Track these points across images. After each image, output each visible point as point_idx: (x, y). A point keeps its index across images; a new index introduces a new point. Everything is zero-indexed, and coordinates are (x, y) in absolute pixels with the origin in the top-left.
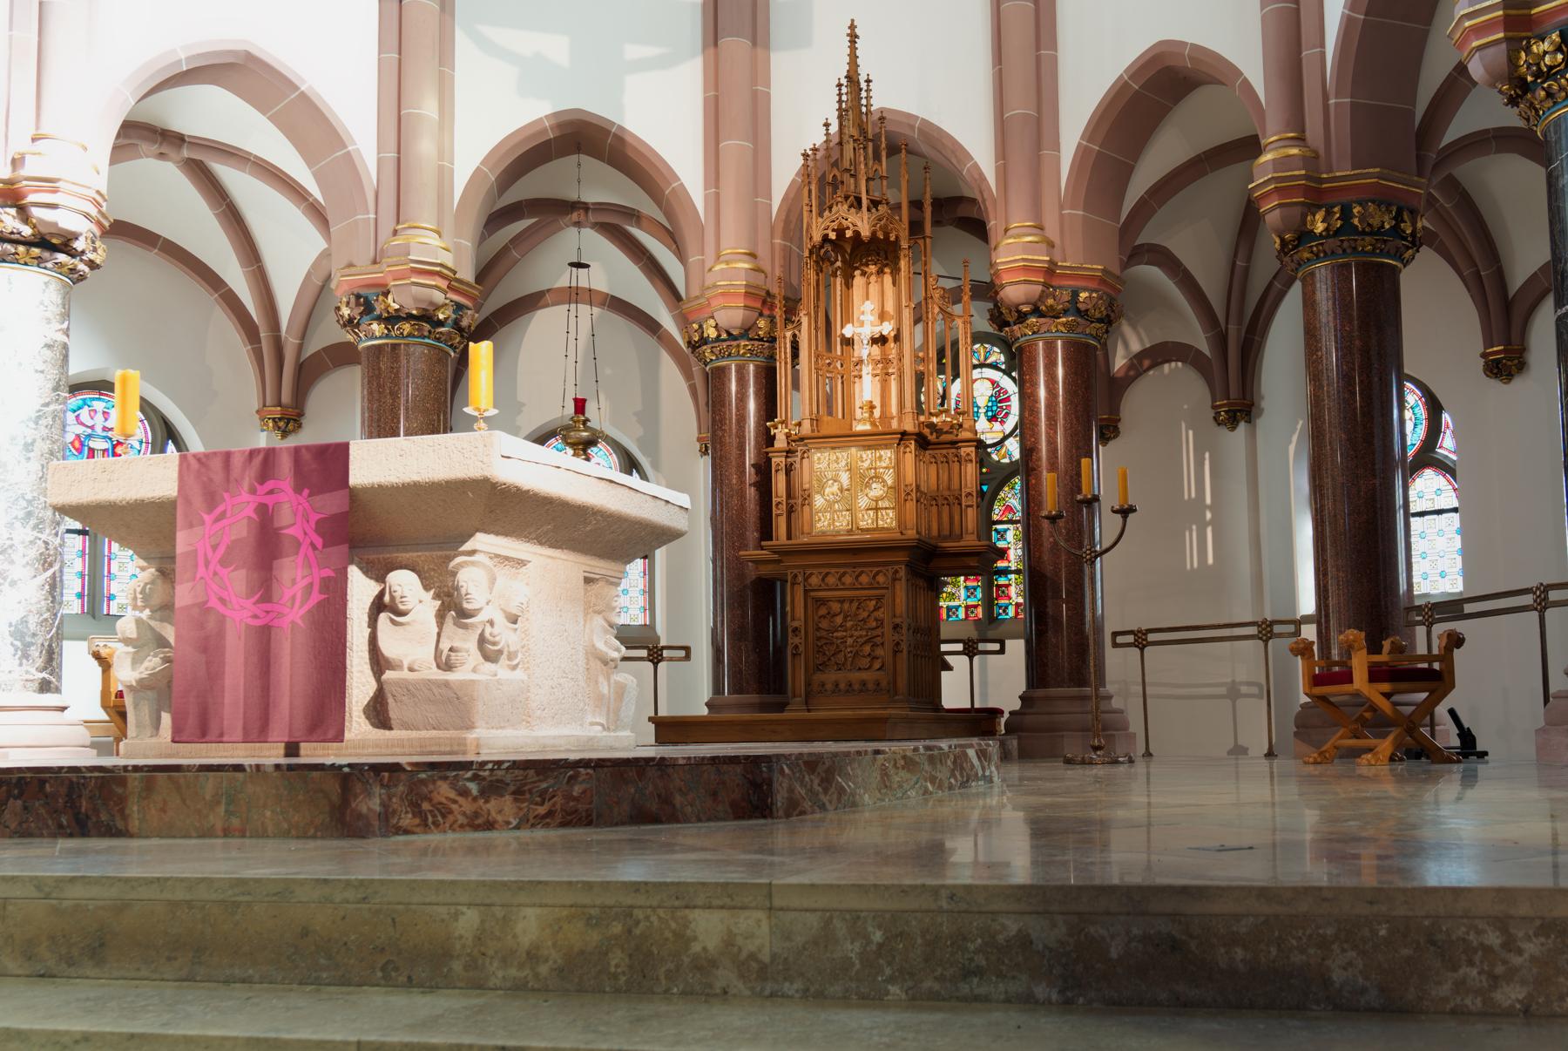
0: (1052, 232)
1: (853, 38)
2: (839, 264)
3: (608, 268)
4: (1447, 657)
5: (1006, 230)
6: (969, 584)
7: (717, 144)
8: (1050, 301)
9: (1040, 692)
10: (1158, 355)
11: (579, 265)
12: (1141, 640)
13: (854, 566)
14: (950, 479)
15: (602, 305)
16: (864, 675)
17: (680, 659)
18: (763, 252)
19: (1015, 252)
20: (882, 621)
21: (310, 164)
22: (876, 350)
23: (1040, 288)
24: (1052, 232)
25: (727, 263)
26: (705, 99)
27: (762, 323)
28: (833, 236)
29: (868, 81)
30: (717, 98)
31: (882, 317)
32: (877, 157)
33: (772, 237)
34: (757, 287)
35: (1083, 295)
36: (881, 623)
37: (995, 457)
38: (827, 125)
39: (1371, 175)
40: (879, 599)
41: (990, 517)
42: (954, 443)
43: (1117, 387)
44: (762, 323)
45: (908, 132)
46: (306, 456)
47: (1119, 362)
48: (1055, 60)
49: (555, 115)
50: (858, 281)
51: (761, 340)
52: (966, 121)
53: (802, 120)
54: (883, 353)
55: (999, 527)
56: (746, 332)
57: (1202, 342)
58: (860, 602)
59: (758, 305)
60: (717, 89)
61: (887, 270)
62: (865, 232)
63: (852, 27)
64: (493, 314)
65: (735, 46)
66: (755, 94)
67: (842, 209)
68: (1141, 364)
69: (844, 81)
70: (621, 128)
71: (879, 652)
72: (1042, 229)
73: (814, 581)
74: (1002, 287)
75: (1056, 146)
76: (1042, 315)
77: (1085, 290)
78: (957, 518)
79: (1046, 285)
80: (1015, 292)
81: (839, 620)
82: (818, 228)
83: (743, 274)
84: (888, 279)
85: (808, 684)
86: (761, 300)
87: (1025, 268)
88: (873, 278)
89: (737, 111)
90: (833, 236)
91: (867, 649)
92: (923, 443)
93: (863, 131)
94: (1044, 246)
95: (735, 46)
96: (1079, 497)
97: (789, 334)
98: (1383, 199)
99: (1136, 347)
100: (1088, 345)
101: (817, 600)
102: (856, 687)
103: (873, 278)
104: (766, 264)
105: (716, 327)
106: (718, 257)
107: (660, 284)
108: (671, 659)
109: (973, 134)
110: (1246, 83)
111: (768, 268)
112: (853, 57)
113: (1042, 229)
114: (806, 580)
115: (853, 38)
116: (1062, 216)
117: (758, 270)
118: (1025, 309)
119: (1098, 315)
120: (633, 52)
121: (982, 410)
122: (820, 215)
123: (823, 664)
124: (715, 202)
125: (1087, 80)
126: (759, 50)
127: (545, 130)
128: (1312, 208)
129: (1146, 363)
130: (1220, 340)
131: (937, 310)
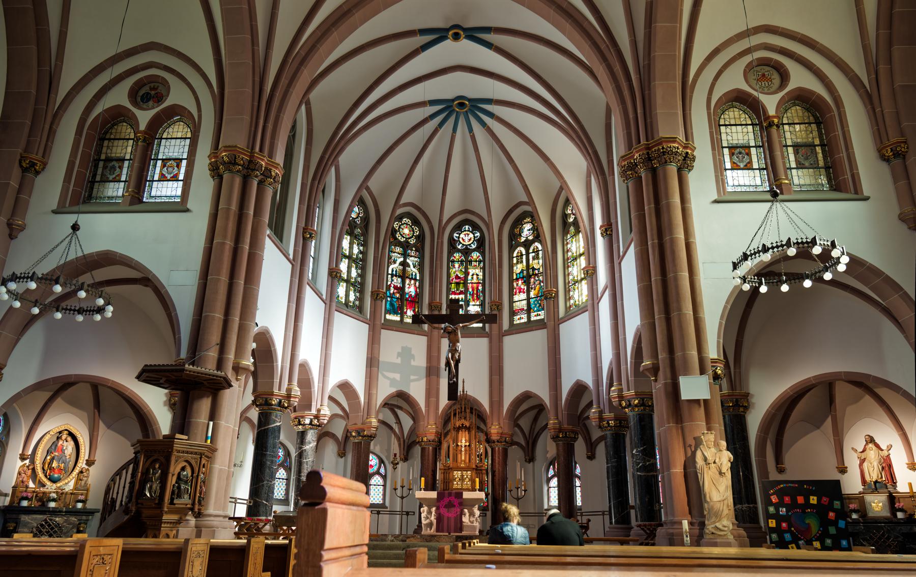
4: (588, 523)
39: (570, 427)
46: (225, 385)
57: (523, 443)
65: (434, 378)
89: (431, 392)
98: (573, 431)
110: (189, 112)
120: (412, 377)
124: (428, 411)
125: (509, 397)
128: (560, 432)
130: (527, 443)
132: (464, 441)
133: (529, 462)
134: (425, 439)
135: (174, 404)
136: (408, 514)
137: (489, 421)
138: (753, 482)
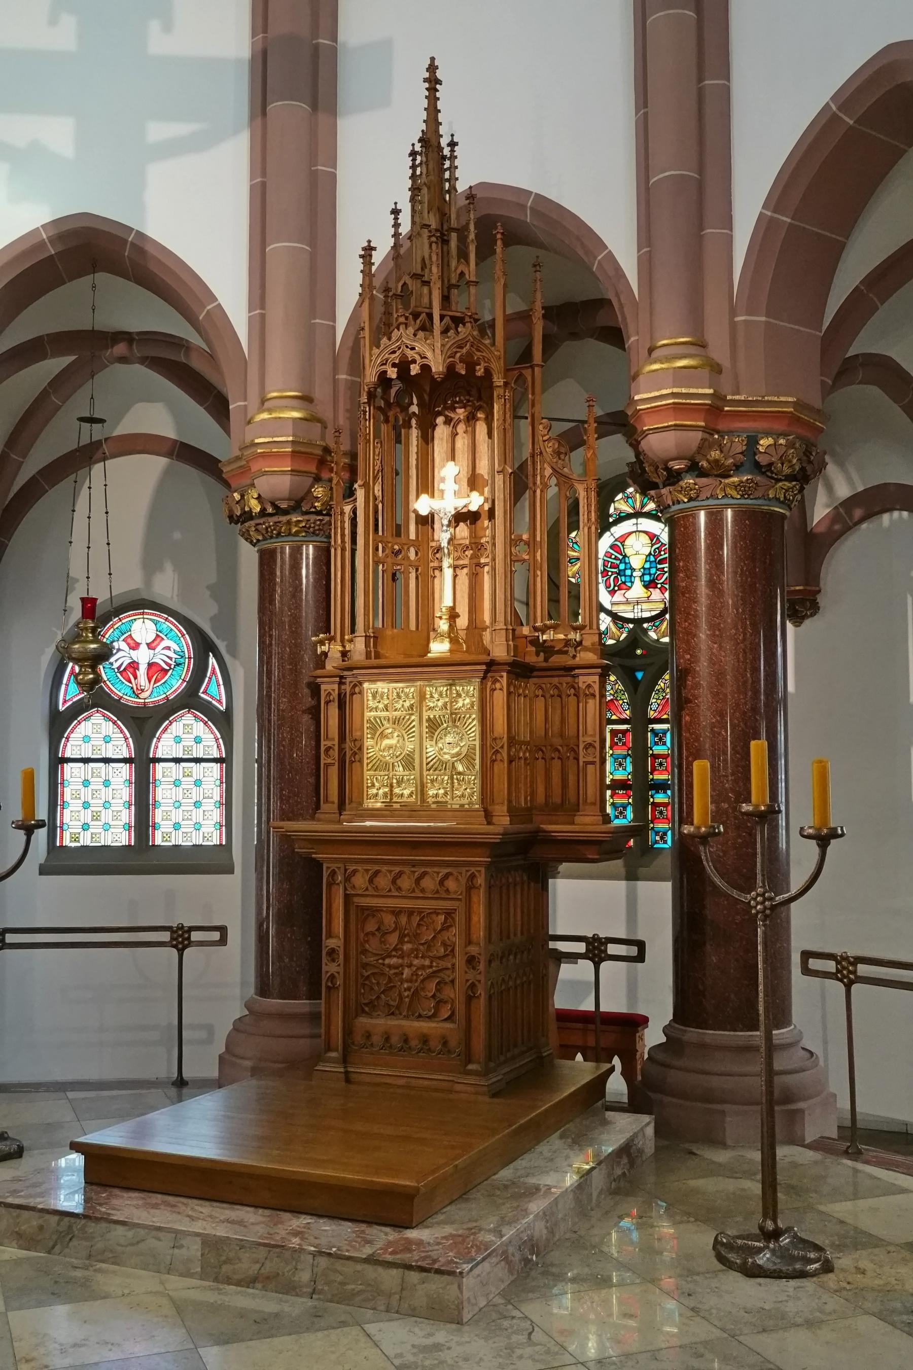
1: (433, 82)
2: (414, 409)
3: (159, 412)
5: (651, 351)
6: (618, 801)
7: (701, 228)
8: (715, 454)
9: (692, 1034)
10: (874, 501)
11: (92, 420)
12: (847, 971)
13: (414, 864)
14: (563, 721)
15: (169, 455)
16: (425, 1026)
18: (322, 393)
19: (661, 381)
22: (463, 531)
23: (699, 435)
24: (719, 352)
26: (252, 188)
27: (319, 491)
29: (453, 144)
31: (474, 482)
32: (463, 255)
33: (335, 370)
34: (310, 444)
35: (765, 442)
37: (653, 635)
38: (396, 212)
40: (449, 914)
41: (646, 713)
42: (568, 670)
43: (816, 546)
44: (319, 491)
45: (515, 214)
47: (820, 512)
48: (726, 93)
49: (55, 222)
50: (441, 431)
51: (319, 513)
52: (598, 191)
53: (372, 207)
54: (475, 536)
55: (657, 727)
56: (297, 504)
58: (425, 916)
59: (313, 468)
60: (264, 174)
62: (438, 367)
63: (432, 68)
64: (40, 472)
67: (404, 335)
68: (850, 514)
69: (418, 148)
70: (140, 235)
72: (704, 346)
73: (360, 881)
74: (645, 434)
75: (728, 222)
76: (702, 473)
77: (767, 434)
78: (572, 778)
79: (708, 430)
81: (393, 939)
82: (377, 362)
83: (290, 428)
84: (481, 428)
85: (348, 1031)
87: (677, 408)
88: (461, 428)
89: (293, 198)
90: (392, 373)
91: (432, 986)
92: (520, 671)
93: (443, 216)
94: (705, 373)
95: (287, 111)
96: (745, 807)
97: (348, 509)
99: (843, 491)
100: (773, 514)
101: (362, 909)
102: (414, 1043)
104: (327, 413)
105: (259, 498)
106: (263, 401)
108: (201, 944)
109: (607, 210)
111: (328, 415)
112: (433, 111)
113: (704, 346)
114: (347, 879)
115: (433, 82)
116: (733, 326)
118: (677, 466)
119: (786, 470)
120: (159, 131)
121: (637, 574)
122: (376, 343)
123: (370, 1003)
124: (259, 326)
126: (322, 117)
127: (41, 245)
129: (858, 513)
131: (548, 471)
136: (181, 939)
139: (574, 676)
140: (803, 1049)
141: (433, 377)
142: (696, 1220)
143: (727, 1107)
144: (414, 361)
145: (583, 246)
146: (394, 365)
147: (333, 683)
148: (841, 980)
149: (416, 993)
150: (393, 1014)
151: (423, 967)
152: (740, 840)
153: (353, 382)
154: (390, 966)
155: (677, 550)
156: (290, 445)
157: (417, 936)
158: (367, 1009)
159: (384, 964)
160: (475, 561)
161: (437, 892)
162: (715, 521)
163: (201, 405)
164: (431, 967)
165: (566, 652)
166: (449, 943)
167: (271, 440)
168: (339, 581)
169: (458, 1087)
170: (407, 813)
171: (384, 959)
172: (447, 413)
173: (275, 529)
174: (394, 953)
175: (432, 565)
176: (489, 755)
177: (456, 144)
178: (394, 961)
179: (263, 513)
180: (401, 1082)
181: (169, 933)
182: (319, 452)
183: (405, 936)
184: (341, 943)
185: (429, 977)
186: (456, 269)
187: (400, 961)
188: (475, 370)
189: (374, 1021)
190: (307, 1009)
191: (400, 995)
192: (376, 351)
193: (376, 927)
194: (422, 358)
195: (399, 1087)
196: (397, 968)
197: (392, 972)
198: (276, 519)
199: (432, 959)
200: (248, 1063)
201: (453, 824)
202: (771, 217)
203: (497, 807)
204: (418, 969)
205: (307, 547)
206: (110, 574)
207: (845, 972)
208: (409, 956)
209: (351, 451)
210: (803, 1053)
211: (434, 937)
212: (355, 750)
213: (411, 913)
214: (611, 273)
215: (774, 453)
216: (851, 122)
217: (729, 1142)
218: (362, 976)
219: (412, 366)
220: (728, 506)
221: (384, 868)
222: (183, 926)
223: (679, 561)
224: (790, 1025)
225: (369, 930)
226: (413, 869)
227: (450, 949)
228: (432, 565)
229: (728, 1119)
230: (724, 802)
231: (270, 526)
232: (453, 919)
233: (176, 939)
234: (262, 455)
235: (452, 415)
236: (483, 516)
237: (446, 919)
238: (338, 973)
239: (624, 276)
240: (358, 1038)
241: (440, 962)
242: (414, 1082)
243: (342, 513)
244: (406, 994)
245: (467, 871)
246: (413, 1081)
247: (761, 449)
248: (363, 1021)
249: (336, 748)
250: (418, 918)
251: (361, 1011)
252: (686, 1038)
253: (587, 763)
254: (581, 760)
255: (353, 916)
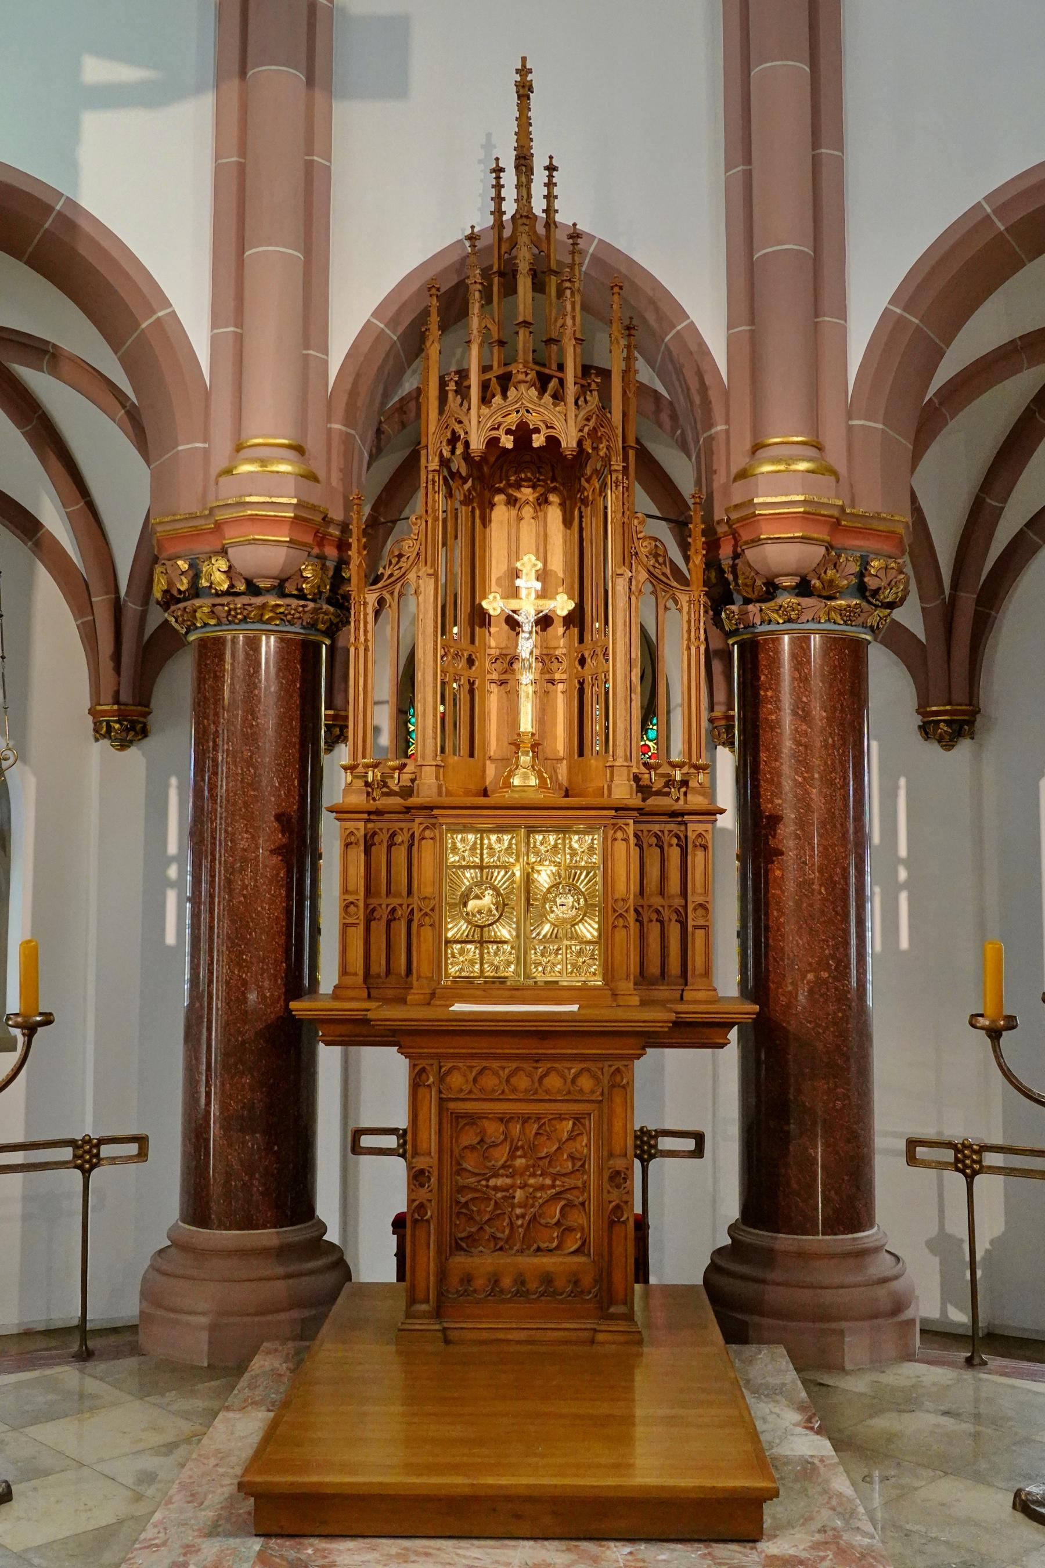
0: (836, 456)
1: (524, 91)
7: (241, 249)
16: (547, 1262)
17: (129, 1159)
20: (584, 1161)
21: (934, 394)
25: (263, 462)
26: (218, 169)
28: (508, 442)
29: (551, 168)
30: (242, 168)
34: (313, 508)
36: (580, 1164)
50: (500, 513)
51: (301, 596)
59: (309, 539)
61: (553, 498)
62: (569, 441)
63: (524, 71)
65: (278, 79)
66: (309, 165)
71: (577, 1218)
73: (456, 1080)
77: (878, 555)
80: (781, 554)
81: (500, 1156)
83: (291, 485)
84: (554, 514)
85: (442, 1275)
86: (312, 526)
89: (787, 249)
90: (508, 442)
91: (555, 1211)
95: (278, 79)
101: (457, 1117)
102: (532, 1285)
103: (528, 511)
106: (239, 448)
107: (53, 459)
108: (113, 1160)
112: (524, 124)
114: (442, 1079)
115: (524, 91)
116: (850, 428)
117: (311, 477)
118: (786, 582)
120: (97, 70)
124: (235, 352)
126: (319, 95)
132: (529, 584)
133: (948, 742)
134: (216, 573)
135: (776, 760)
136: (87, 1155)
137: (730, 430)
138: (882, 936)
139: (685, 824)
140: (887, 1251)
141: (561, 454)
142: (946, 1473)
143: (844, 1325)
144: (537, 431)
145: (657, 309)
146: (508, 432)
147: (359, 820)
148: (963, 1172)
149: (534, 1219)
150: (501, 1249)
151: (542, 1188)
152: (840, 1015)
153: (348, 434)
154: (496, 1188)
155: (763, 678)
156: (291, 508)
157: (533, 1147)
158: (464, 1245)
159: (487, 1186)
160: (547, 676)
161: (569, 1092)
162: (801, 644)
163: (19, 426)
164: (553, 1186)
165: (668, 794)
166: (578, 1155)
167: (268, 499)
168: (361, 689)
169: (600, 1337)
170: (507, 992)
171: (488, 1180)
172: (510, 491)
173: (241, 613)
174: (501, 1171)
175: (489, 677)
176: (610, 922)
177: (555, 169)
178: (499, 1182)
179: (230, 593)
180: (522, 1335)
181: (70, 1149)
182: (318, 519)
183: (517, 1149)
184: (434, 1161)
185: (556, 1197)
186: (556, 321)
187: (508, 1181)
188: (531, 440)
189: (476, 1260)
190: (275, 1242)
191: (511, 1224)
192: (485, 410)
193: (479, 1138)
194: (547, 427)
195: (519, 1342)
196: (507, 1190)
197: (499, 1195)
198: (245, 599)
199: (554, 1177)
200: (204, 1320)
201: (575, 1008)
202: (901, 316)
203: (620, 983)
204: (536, 1189)
205: (268, 639)
206: (3, 658)
207: (968, 1162)
208: (522, 1174)
209: (343, 522)
210: (888, 1256)
211: (559, 1148)
212: (428, 910)
213: (525, 1120)
214: (694, 348)
215: (884, 578)
216: (1002, 228)
217: (848, 1366)
218: (458, 1203)
219: (534, 436)
220: (815, 632)
221: (495, 1065)
222: (90, 1140)
223: (767, 690)
224: (872, 1226)
225: (466, 1143)
226: (535, 1065)
227: (579, 1163)
228: (489, 677)
229: (847, 1339)
230: (825, 970)
231: (235, 609)
232: (584, 1125)
233: (81, 1157)
234: (253, 518)
235: (518, 495)
236: (555, 621)
237: (574, 1124)
238: (430, 1201)
239: (708, 353)
240: (454, 1281)
241: (567, 1180)
242: (538, 1335)
243: (365, 604)
244: (520, 1222)
245: (610, 1066)
246: (539, 1333)
247: (873, 571)
248: (459, 1262)
249: (361, 905)
250: (536, 1126)
251: (457, 1247)
252: (778, 1246)
253: (695, 927)
254: (690, 923)
255: (446, 1126)
